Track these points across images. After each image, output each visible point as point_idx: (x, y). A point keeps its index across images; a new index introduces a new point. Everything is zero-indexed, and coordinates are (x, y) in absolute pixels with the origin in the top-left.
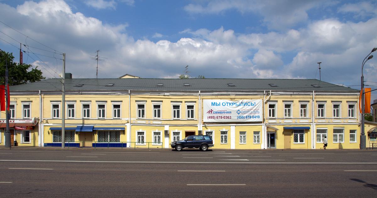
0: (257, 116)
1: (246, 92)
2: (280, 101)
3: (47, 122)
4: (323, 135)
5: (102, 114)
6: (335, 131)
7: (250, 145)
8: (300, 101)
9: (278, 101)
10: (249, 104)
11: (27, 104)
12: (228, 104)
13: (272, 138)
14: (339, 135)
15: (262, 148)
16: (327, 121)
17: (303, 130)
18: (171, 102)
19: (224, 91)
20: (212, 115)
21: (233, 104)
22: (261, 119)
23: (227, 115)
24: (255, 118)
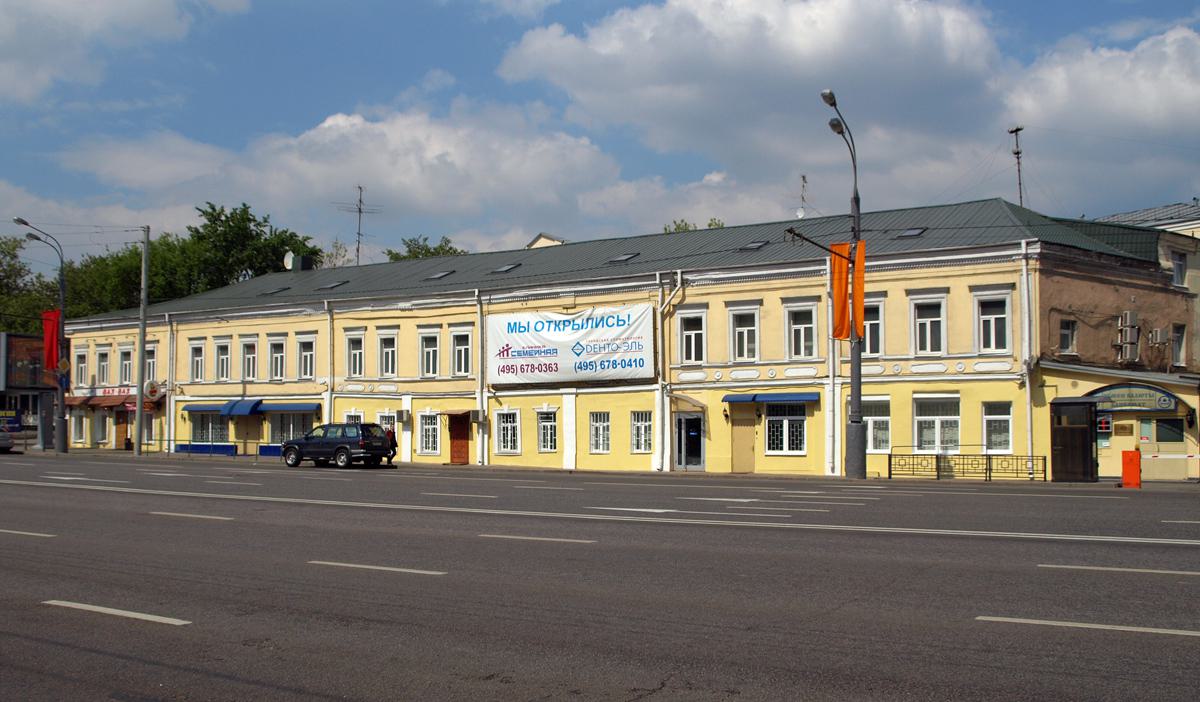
0: (635, 361)
1: (767, 269)
3: (182, 392)
4: (875, 423)
6: (923, 407)
7: (621, 457)
8: (728, 304)
9: (951, 291)
10: (611, 321)
12: (553, 326)
13: (691, 433)
14: (944, 424)
15: (654, 467)
16: (890, 368)
17: (804, 406)
18: (419, 326)
19: (540, 286)
20: (510, 362)
21: (567, 323)
22: (648, 371)
23: (546, 360)
24: (631, 365)
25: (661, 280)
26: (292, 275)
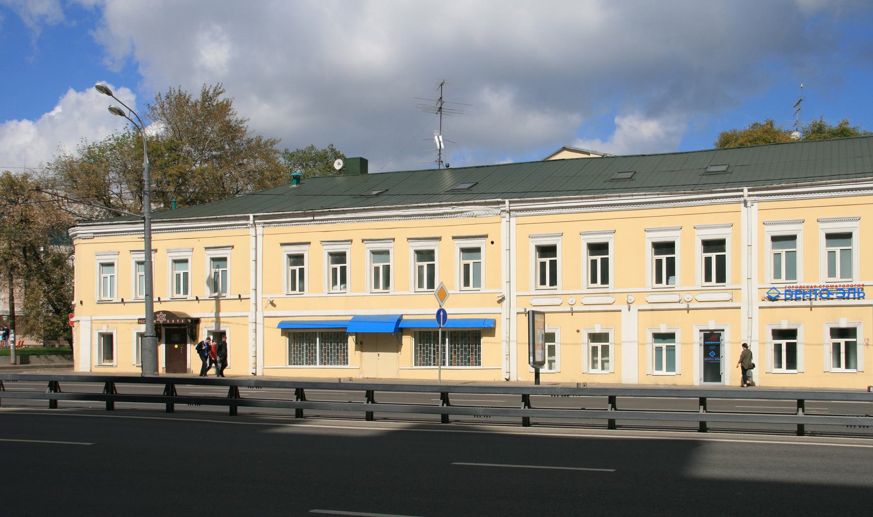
2: (401, 241)
5: (382, 278)
11: (295, 250)
25: (254, 221)
26: (340, 179)
